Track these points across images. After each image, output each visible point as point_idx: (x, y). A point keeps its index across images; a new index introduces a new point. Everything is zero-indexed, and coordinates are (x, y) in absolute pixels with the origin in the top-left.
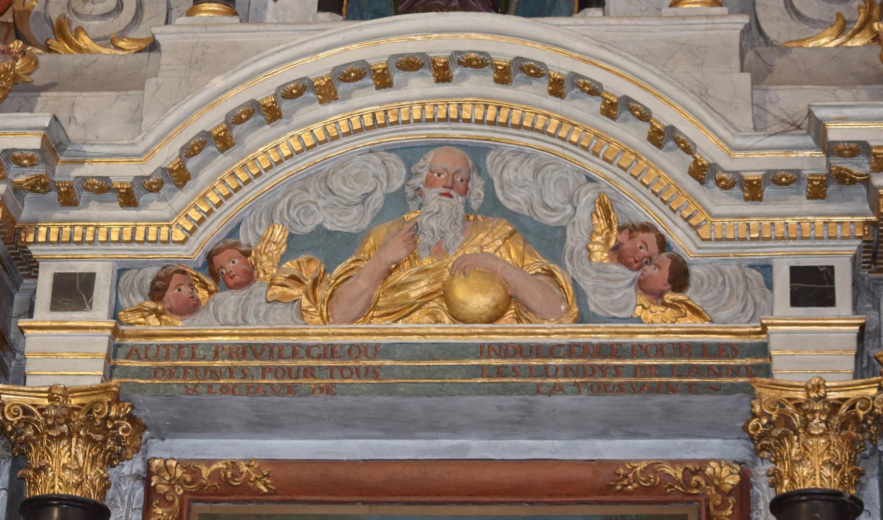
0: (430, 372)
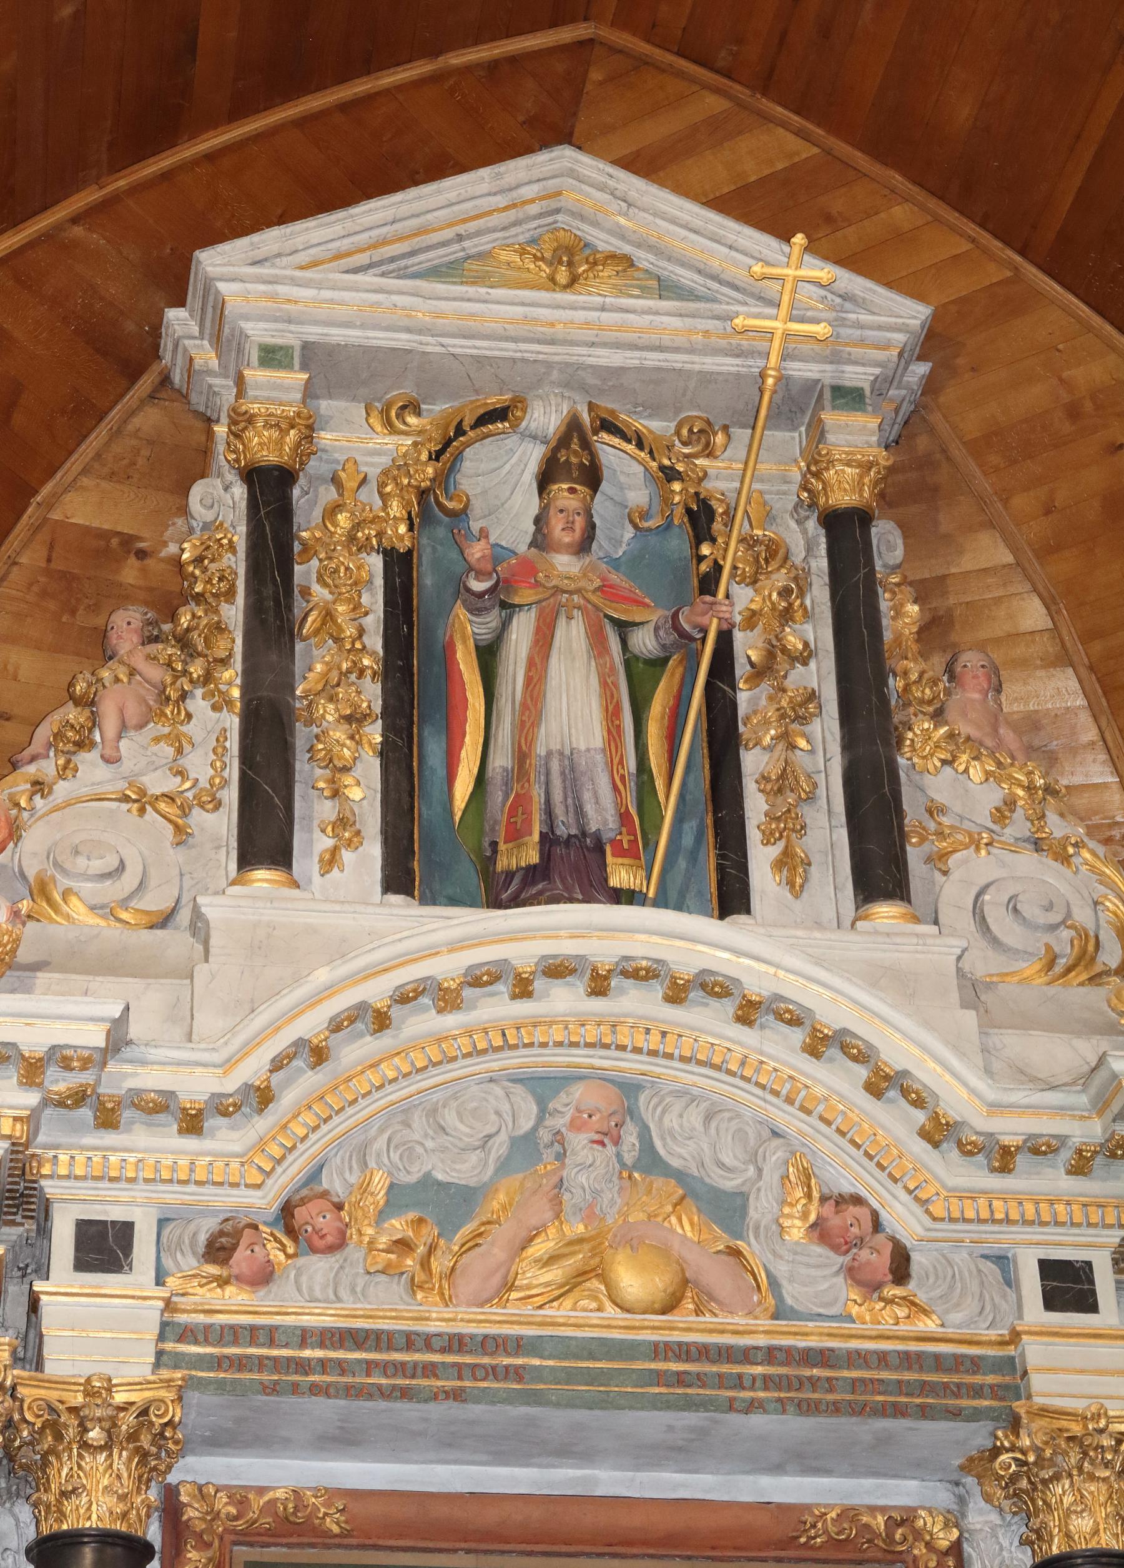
0: (592, 1377)
